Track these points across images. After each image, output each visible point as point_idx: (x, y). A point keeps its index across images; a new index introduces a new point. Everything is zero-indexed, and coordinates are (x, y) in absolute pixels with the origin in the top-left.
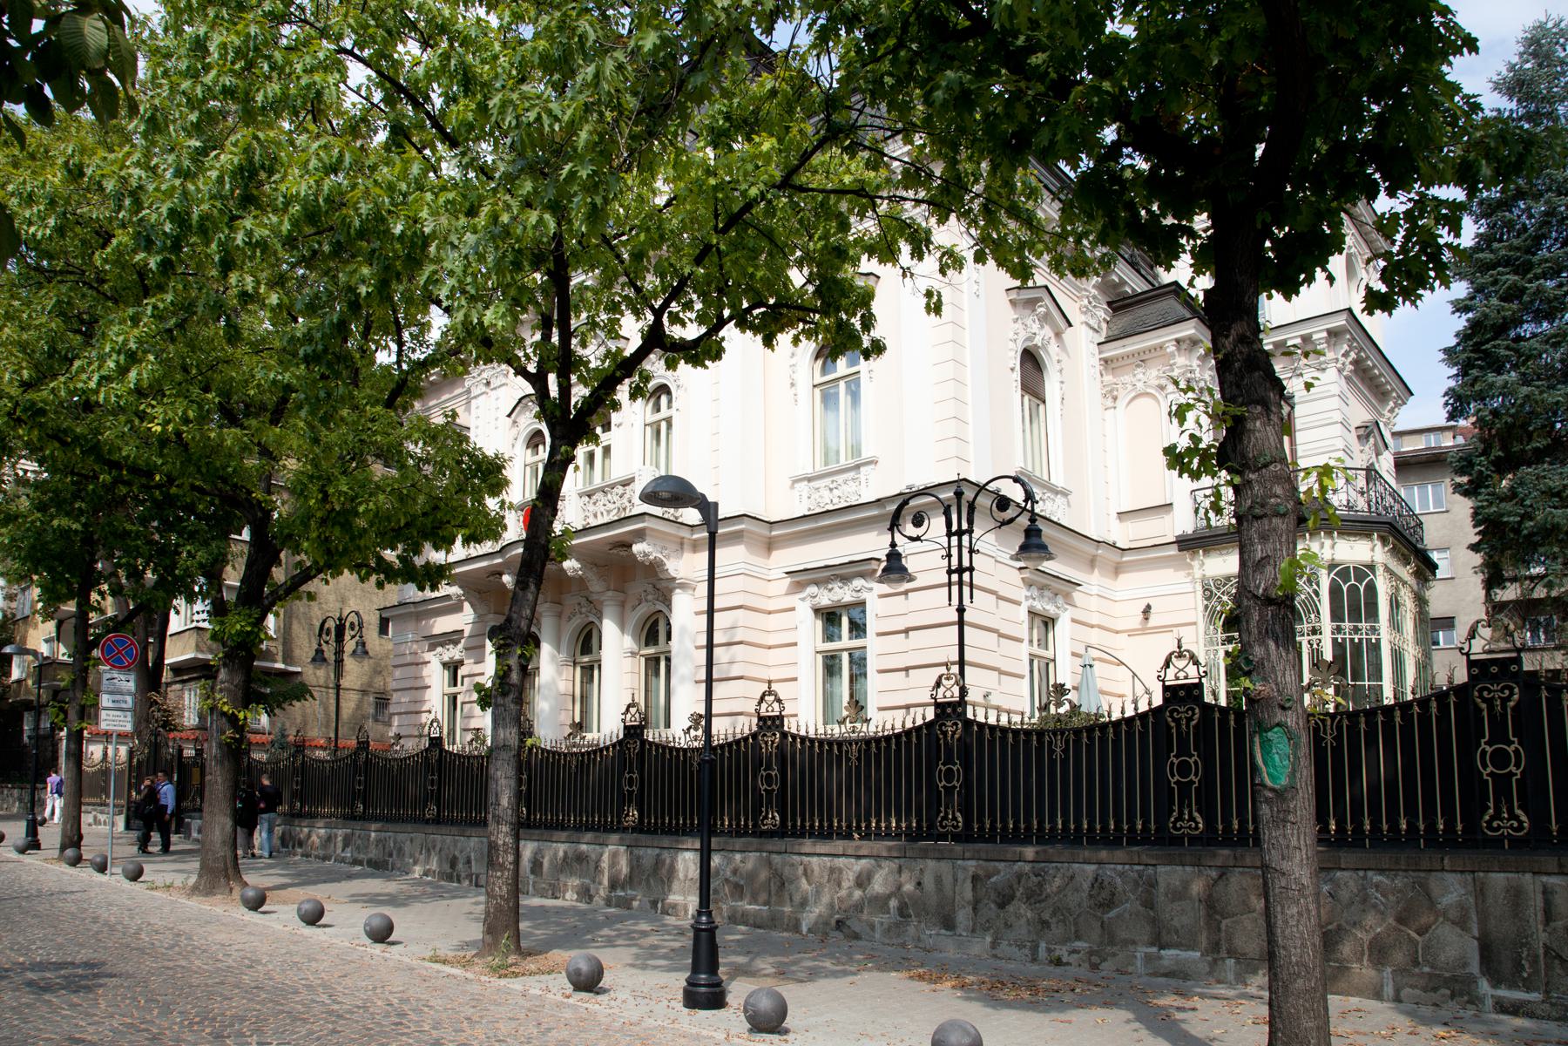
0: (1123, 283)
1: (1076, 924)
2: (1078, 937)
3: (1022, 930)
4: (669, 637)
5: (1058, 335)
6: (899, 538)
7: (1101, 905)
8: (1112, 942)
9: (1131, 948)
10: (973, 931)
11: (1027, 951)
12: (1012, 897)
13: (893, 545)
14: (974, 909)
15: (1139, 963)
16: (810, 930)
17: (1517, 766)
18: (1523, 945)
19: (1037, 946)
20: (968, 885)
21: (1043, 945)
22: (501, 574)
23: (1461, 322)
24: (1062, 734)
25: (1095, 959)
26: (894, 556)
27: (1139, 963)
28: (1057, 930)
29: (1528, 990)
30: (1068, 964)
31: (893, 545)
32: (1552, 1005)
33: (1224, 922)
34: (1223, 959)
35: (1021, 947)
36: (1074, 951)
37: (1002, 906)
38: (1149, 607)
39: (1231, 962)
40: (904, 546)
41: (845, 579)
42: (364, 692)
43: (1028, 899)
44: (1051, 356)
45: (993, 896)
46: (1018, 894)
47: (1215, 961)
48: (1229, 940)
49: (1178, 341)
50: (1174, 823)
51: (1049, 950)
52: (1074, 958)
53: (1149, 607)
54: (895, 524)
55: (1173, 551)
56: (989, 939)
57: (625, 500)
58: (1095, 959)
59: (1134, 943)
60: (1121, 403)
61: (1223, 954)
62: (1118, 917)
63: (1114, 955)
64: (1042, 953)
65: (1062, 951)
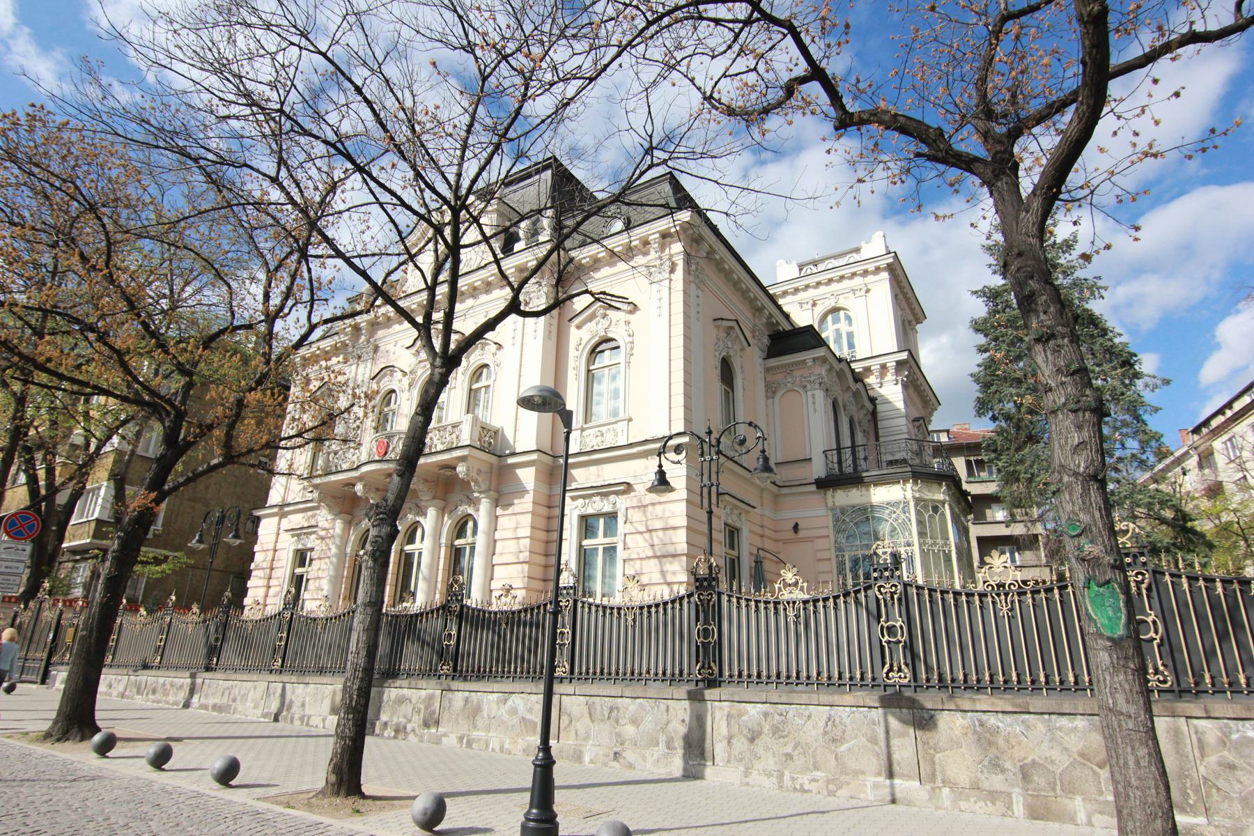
0: (778, 323)
1: (814, 756)
2: (816, 768)
3: (770, 762)
4: (475, 533)
5: (742, 349)
6: (664, 461)
7: (834, 740)
8: (845, 772)
9: (861, 777)
10: (729, 761)
11: (774, 780)
12: (760, 733)
13: (660, 466)
14: (729, 742)
15: (869, 791)
16: (591, 761)
17: (1156, 632)
18: (1186, 777)
19: (782, 775)
20: (724, 724)
21: (787, 773)
22: (354, 485)
23: (981, 358)
24: (794, 603)
25: (831, 787)
26: (661, 474)
27: (869, 791)
28: (799, 761)
29: (1195, 815)
30: (808, 791)
31: (660, 466)
32: (1216, 827)
33: (938, 756)
34: (940, 788)
35: (769, 775)
36: (814, 780)
37: (752, 740)
38: (797, 525)
39: (946, 791)
40: (667, 467)
41: (605, 495)
42: (225, 571)
43: (774, 734)
44: (736, 363)
45: (745, 732)
46: (765, 731)
47: (933, 789)
48: (943, 772)
49: (814, 359)
50: (887, 673)
51: (793, 779)
52: (813, 786)
53: (797, 525)
54: (659, 455)
55: (813, 488)
56: (742, 768)
57: (454, 436)
58: (831, 787)
59: (863, 773)
60: (778, 396)
61: (939, 783)
62: (849, 750)
63: (848, 783)
64: (787, 781)
65: (804, 780)
